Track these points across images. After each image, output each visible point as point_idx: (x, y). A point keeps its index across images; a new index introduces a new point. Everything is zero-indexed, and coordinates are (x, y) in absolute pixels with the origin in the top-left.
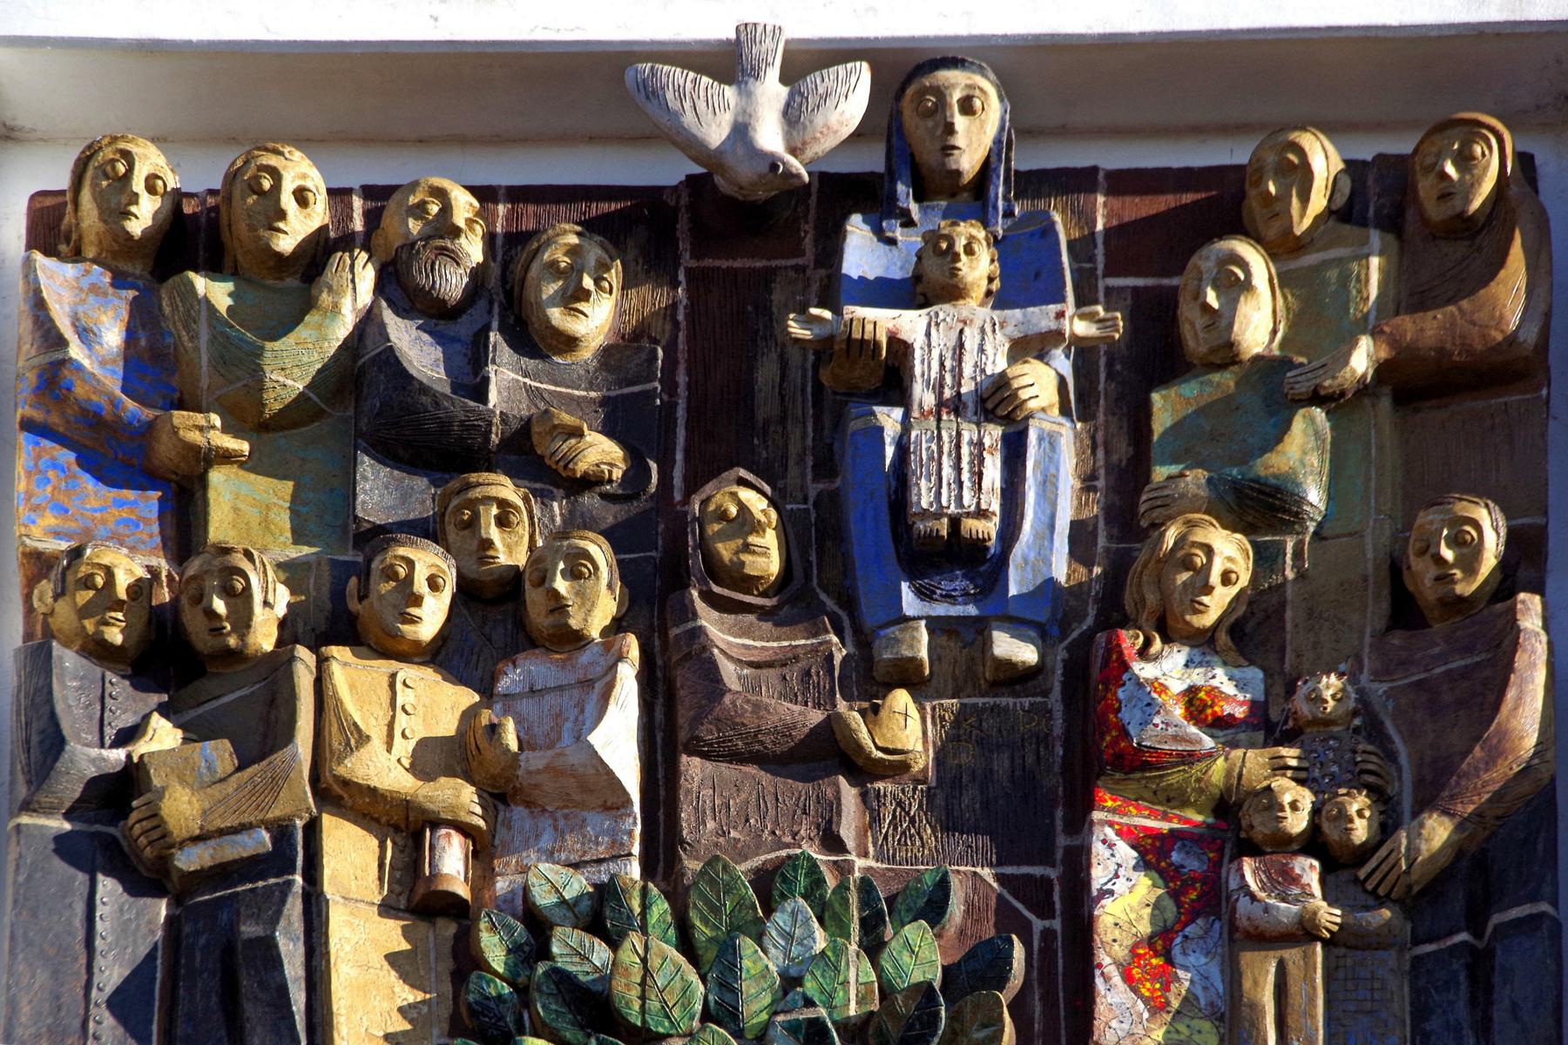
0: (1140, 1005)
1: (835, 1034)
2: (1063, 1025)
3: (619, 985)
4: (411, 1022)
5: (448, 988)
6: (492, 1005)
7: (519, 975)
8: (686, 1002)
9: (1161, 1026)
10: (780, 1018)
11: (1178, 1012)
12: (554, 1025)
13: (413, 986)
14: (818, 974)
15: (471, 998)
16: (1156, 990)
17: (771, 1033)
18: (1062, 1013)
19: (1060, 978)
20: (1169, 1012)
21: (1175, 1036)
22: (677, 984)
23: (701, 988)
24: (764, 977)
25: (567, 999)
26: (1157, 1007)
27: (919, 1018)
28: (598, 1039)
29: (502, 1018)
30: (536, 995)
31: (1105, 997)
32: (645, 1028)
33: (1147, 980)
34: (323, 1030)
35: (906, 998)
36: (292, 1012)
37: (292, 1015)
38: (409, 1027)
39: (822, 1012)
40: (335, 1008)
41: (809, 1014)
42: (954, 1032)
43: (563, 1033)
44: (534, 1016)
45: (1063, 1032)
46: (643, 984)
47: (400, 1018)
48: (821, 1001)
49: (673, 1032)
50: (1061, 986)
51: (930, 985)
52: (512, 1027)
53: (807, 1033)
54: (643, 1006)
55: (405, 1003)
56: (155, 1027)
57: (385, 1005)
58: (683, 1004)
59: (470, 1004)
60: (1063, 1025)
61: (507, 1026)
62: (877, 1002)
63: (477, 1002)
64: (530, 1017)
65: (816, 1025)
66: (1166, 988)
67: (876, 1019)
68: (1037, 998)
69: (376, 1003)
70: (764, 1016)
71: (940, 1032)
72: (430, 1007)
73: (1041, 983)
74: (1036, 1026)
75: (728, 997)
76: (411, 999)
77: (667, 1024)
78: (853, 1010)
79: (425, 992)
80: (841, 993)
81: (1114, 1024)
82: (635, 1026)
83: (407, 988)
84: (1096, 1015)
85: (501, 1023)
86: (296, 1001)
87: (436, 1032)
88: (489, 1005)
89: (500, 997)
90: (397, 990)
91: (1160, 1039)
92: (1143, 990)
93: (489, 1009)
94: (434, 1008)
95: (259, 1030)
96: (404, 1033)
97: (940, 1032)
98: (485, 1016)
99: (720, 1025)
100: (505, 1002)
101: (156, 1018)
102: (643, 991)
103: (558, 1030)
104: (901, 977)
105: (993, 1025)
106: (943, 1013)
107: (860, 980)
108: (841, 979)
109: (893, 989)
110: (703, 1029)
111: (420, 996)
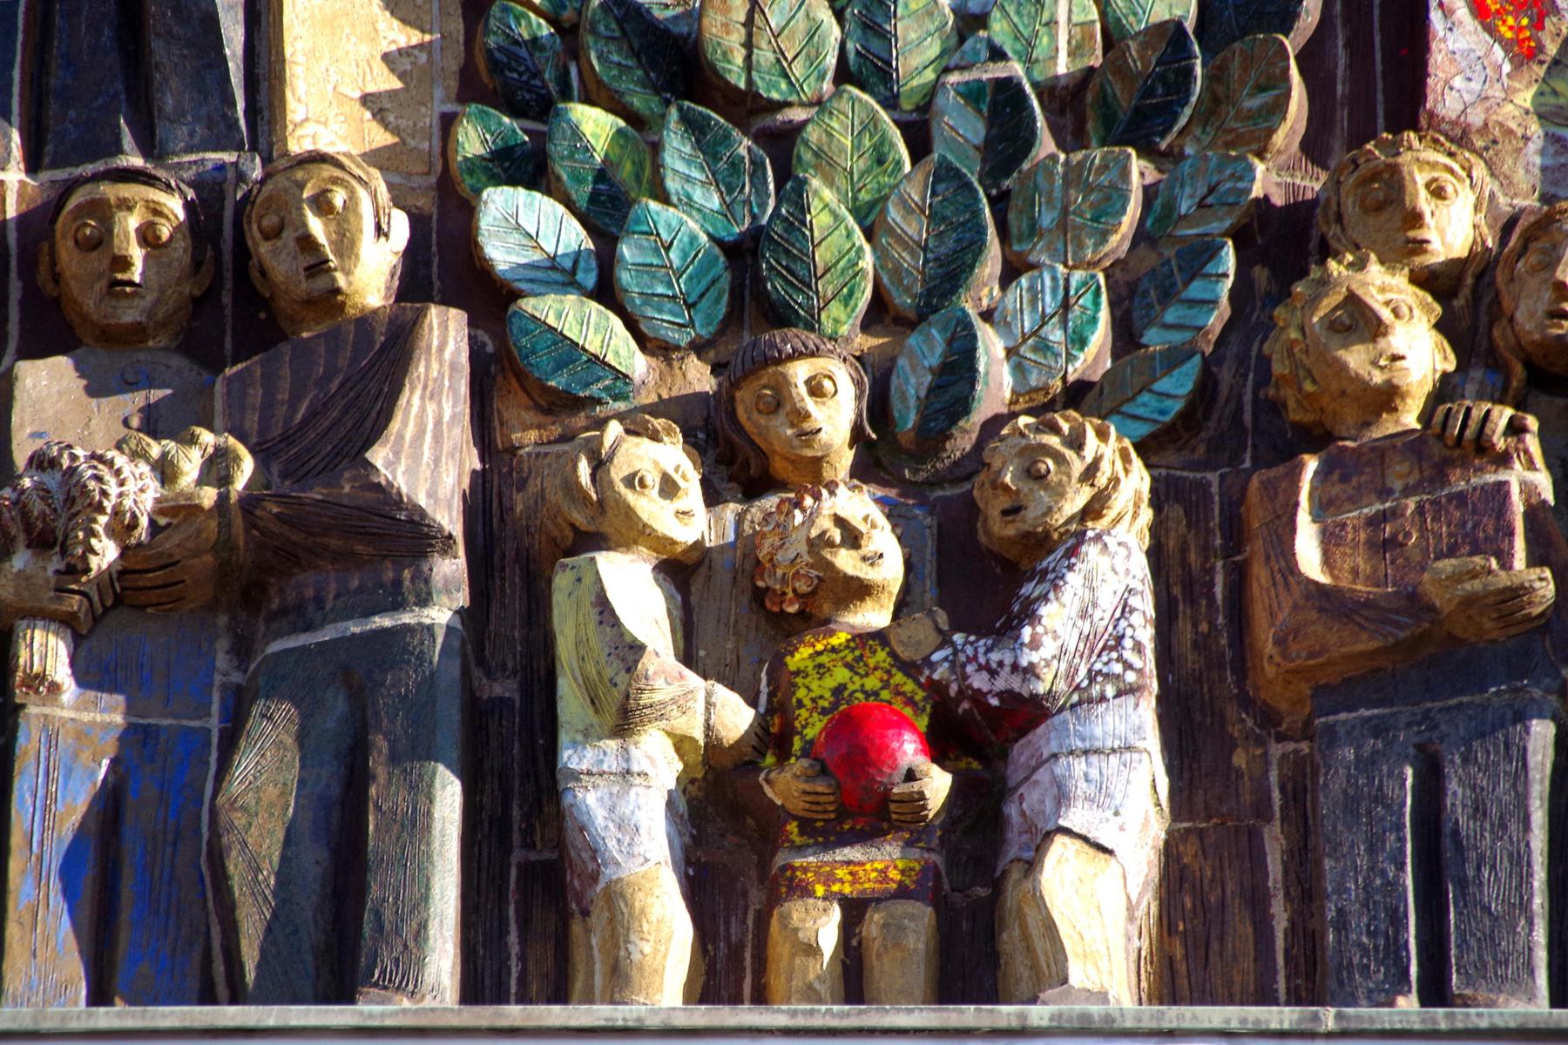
0: (1498, 52)
1: (1035, 104)
2: (1380, 85)
3: (712, 25)
4: (401, 77)
5: (457, 25)
6: (523, 52)
7: (564, 7)
8: (813, 53)
9: (1529, 84)
10: (954, 78)
11: (1556, 62)
12: (615, 85)
13: (405, 21)
14: (1011, 9)
15: (492, 41)
16: (1521, 29)
17: (940, 100)
18: (1379, 68)
19: (1376, 12)
20: (1541, 63)
21: (1552, 100)
22: (800, 24)
23: (836, 32)
24: (930, 14)
25: (636, 45)
26: (1524, 53)
27: (1162, 77)
28: (680, 109)
29: (537, 74)
30: (590, 40)
31: (1444, 40)
32: (751, 93)
33: (1511, 13)
34: (270, 86)
35: (1144, 46)
36: (225, 56)
37: (223, 60)
38: (397, 84)
39: (1017, 68)
40: (288, 51)
41: (997, 71)
42: (1216, 100)
43: (628, 98)
44: (586, 71)
45: (1380, 97)
46: (749, 23)
47: (386, 71)
48: (1015, 52)
49: (793, 98)
50: (1377, 25)
51: (1178, 25)
52: (553, 88)
53: (994, 105)
54: (748, 58)
55: (393, 47)
56: (16, 74)
57: (364, 50)
58: (808, 55)
59: (489, 51)
60: (1380, 85)
61: (544, 86)
62: (1099, 52)
63: (500, 49)
64: (580, 72)
65: (1008, 90)
66: (1538, 25)
67: (1097, 80)
68: (1340, 43)
69: (350, 47)
70: (930, 75)
71: (1194, 99)
72: (430, 54)
73: (1347, 20)
74: (1339, 87)
75: (876, 45)
76: (403, 42)
77: (784, 86)
78: (1063, 66)
79: (423, 31)
80: (1045, 40)
81: (1458, 82)
82: (736, 89)
83: (396, 23)
84: (1431, 70)
85: (537, 82)
86: (230, 40)
87: (438, 93)
88: (517, 53)
89: (535, 40)
90: (381, 26)
91: (1528, 105)
92: (1503, 29)
93: (518, 58)
94: (437, 56)
95: (174, 83)
96: (392, 94)
97: (1194, 99)
98: (512, 70)
99: (863, 88)
100: (542, 48)
101: (18, 58)
102: (750, 35)
103: (622, 94)
104: (1135, 14)
105: (1274, 88)
106: (1199, 70)
107: (1075, 19)
108: (1046, 17)
109: (1124, 34)
110: (838, 94)
111: (415, 37)
